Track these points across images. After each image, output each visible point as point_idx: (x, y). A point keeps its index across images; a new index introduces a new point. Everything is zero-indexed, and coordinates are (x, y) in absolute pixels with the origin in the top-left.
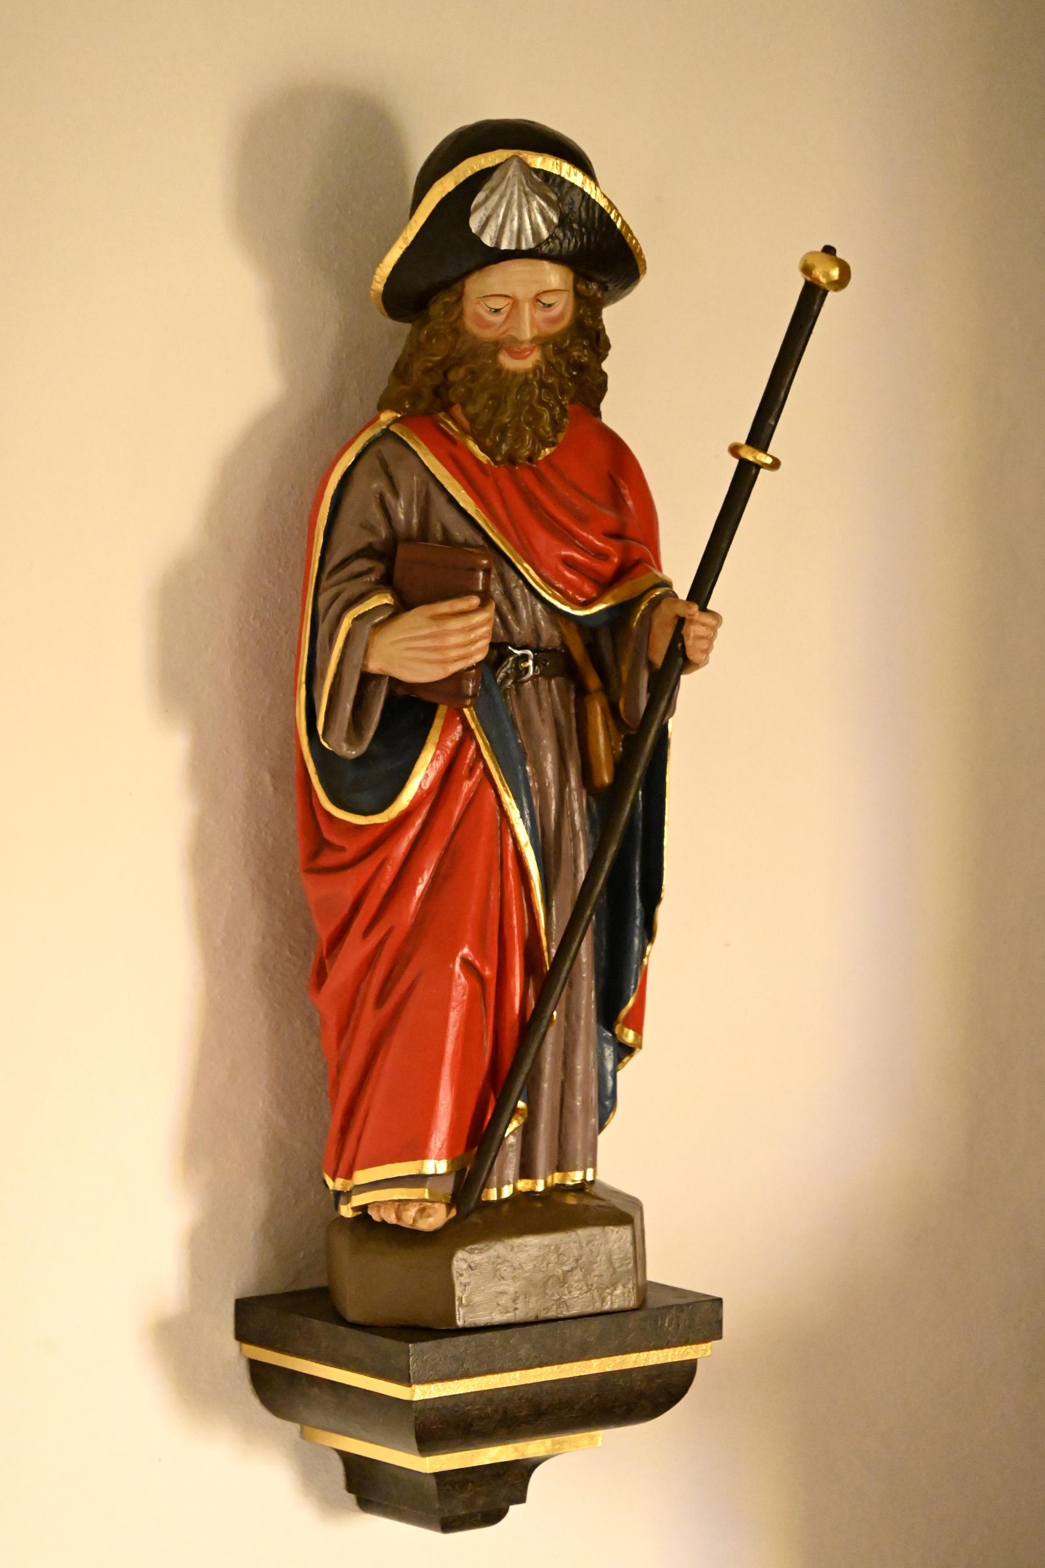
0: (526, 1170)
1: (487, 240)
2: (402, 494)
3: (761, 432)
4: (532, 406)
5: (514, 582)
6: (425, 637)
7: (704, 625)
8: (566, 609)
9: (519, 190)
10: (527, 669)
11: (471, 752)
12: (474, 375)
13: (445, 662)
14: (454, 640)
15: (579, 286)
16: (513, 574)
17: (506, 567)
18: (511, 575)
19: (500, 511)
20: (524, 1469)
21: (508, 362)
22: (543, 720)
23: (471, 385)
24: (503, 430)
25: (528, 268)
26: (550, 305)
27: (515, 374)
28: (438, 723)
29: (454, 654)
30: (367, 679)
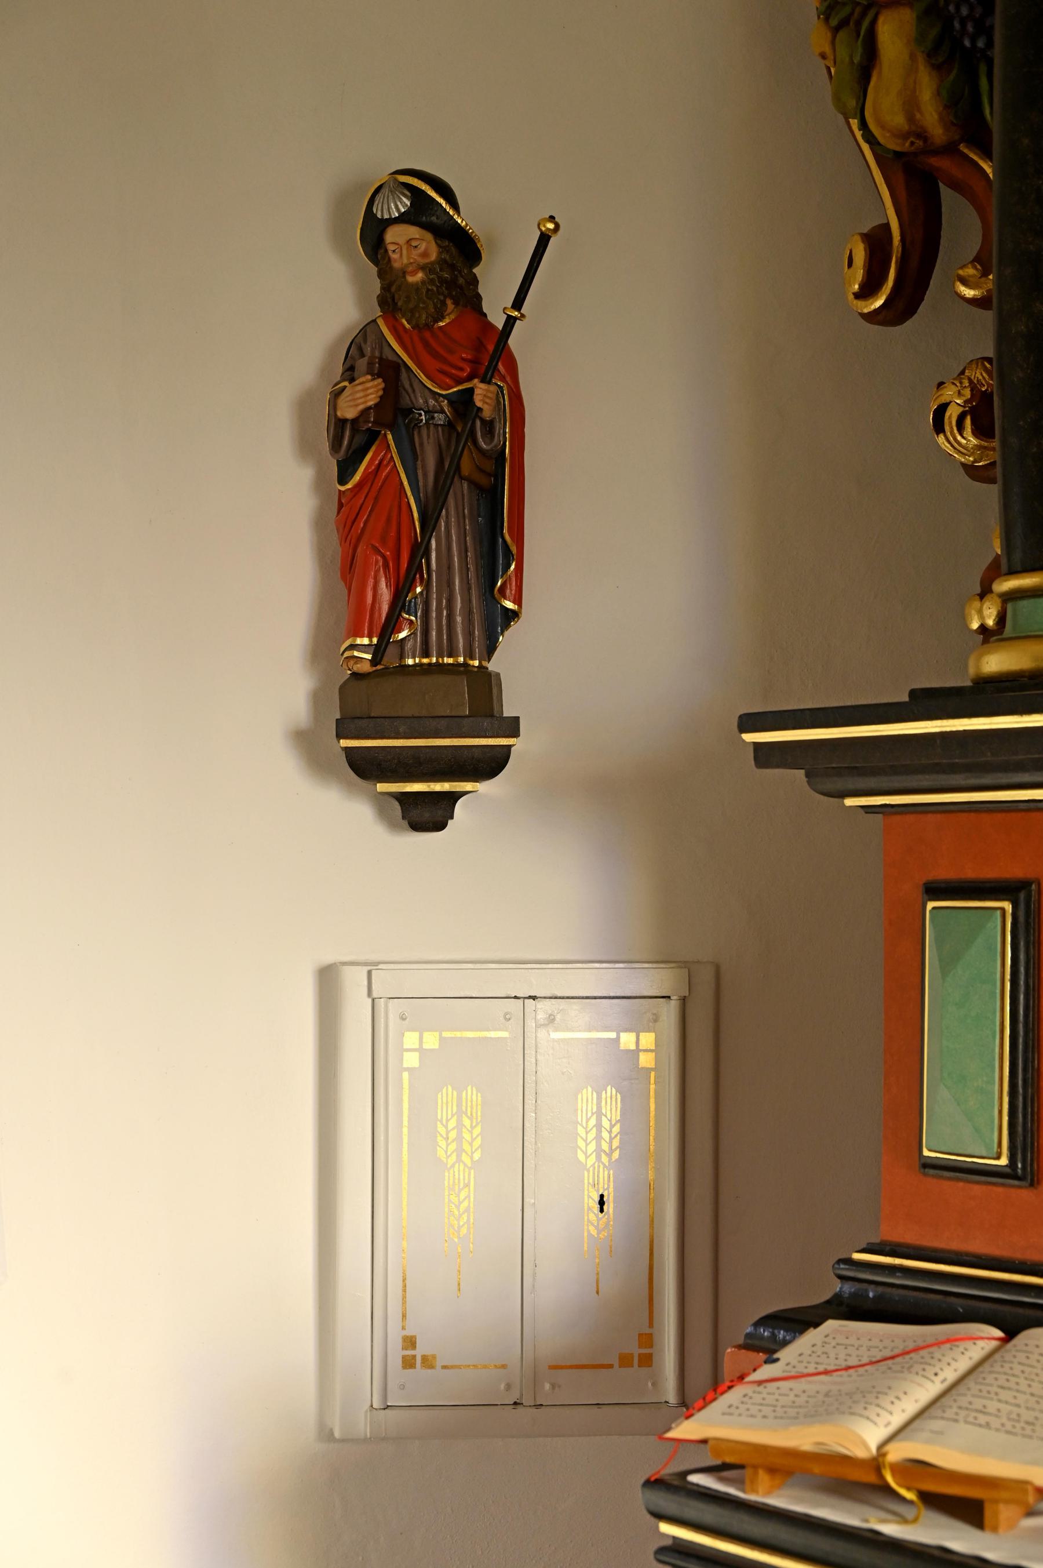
0: (426, 654)
2: (369, 343)
5: (412, 376)
13: (357, 405)
14: (359, 395)
20: (453, 798)
21: (410, 279)
28: (377, 443)
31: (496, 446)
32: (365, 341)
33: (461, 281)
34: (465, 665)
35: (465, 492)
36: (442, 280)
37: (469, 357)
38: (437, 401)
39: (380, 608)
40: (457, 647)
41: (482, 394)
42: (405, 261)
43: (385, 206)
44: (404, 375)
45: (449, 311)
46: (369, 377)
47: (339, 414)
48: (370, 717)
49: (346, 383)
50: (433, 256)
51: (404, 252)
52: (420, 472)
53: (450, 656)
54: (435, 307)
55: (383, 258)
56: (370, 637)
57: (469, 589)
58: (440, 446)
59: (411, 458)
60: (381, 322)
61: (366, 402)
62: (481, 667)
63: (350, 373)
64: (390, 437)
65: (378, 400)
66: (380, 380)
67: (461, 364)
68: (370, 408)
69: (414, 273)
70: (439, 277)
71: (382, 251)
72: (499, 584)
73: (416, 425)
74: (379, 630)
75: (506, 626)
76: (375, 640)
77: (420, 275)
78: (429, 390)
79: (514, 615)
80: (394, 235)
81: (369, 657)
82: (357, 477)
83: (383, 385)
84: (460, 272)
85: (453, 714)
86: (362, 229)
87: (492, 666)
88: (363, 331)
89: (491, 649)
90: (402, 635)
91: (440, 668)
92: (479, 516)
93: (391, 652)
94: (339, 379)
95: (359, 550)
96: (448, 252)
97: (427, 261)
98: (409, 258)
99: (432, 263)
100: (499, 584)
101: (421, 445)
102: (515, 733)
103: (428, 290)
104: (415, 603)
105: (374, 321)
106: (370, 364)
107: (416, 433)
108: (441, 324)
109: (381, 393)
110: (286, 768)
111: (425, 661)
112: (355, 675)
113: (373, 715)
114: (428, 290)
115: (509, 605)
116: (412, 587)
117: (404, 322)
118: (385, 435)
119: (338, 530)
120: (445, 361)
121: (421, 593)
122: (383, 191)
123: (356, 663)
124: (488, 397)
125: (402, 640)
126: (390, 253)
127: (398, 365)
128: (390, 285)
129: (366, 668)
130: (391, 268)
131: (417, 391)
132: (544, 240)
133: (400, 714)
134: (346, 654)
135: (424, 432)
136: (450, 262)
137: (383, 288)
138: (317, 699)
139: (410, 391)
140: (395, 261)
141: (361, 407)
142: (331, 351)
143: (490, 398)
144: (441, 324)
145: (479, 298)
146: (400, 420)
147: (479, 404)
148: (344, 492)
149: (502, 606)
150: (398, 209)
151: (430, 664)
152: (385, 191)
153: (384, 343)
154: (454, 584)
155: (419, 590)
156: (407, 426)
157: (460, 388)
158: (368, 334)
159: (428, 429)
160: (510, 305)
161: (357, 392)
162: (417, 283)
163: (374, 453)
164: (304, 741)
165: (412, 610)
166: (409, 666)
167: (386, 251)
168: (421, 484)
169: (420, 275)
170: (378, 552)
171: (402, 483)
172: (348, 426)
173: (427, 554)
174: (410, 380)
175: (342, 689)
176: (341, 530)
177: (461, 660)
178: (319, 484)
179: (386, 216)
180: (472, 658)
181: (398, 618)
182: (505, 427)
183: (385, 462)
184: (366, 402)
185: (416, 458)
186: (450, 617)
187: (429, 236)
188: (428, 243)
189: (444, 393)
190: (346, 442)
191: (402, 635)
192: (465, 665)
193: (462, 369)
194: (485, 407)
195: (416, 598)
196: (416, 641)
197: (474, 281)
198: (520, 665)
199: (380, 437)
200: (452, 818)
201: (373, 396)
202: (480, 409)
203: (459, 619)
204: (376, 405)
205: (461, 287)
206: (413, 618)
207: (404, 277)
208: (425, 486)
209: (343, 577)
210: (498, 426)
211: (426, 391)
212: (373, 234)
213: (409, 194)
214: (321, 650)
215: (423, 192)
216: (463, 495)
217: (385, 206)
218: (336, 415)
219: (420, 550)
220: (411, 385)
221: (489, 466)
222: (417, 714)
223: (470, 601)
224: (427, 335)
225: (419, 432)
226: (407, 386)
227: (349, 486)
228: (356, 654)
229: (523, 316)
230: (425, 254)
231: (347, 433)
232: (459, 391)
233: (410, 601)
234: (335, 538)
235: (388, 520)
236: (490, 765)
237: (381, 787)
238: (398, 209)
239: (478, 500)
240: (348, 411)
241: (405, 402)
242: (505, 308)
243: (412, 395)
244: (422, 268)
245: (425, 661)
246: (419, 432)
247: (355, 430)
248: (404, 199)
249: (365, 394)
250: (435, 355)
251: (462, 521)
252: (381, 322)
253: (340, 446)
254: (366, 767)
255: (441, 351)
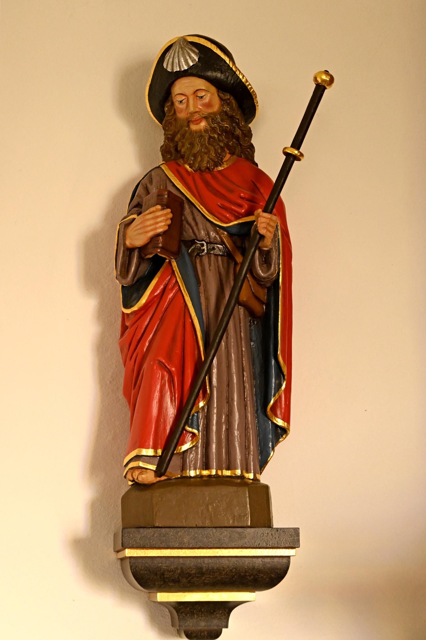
0: (207, 466)
1: (169, 70)
2: (154, 184)
3: (297, 142)
4: (206, 145)
5: (195, 211)
7: (264, 217)
8: (218, 223)
10: (204, 250)
11: (174, 281)
12: (183, 136)
14: (148, 223)
15: (220, 94)
16: (196, 210)
17: (194, 208)
18: (195, 211)
19: (195, 191)
20: (227, 608)
21: (194, 127)
24: (195, 156)
28: (162, 270)
29: (149, 228)
31: (272, 274)
32: (151, 182)
33: (238, 132)
34: (242, 477)
35: (242, 317)
36: (224, 130)
37: (246, 196)
38: (217, 233)
39: (165, 422)
40: (235, 460)
41: (264, 221)
42: (192, 109)
43: (176, 60)
44: (187, 210)
45: (225, 159)
46: (159, 207)
47: (128, 243)
48: (155, 527)
53: (228, 469)
56: (155, 448)
57: (246, 406)
59: (195, 283)
61: (156, 229)
62: (255, 479)
63: (137, 206)
64: (174, 264)
65: (166, 228)
66: (169, 210)
67: (240, 201)
68: (158, 235)
70: (220, 127)
71: (169, 104)
72: (272, 402)
73: (198, 254)
74: (164, 442)
75: (276, 441)
76: (160, 452)
77: (203, 124)
78: (210, 226)
79: (284, 431)
80: (183, 87)
81: (154, 467)
83: (171, 216)
85: (236, 524)
86: (151, 85)
87: (264, 479)
88: (149, 176)
89: (263, 463)
90: (185, 447)
91: (218, 480)
92: (251, 340)
93: (176, 461)
95: (145, 366)
96: (228, 104)
97: (210, 111)
98: (195, 106)
99: (214, 114)
100: (272, 402)
101: (203, 271)
102: (294, 544)
103: (210, 137)
104: (198, 417)
105: (159, 167)
106: (160, 195)
107: (198, 261)
108: (220, 168)
109: (169, 222)
110: (65, 574)
111: (205, 473)
112: (137, 486)
113: (157, 524)
114: (210, 137)
115: (280, 422)
116: (195, 403)
118: (170, 263)
119: (122, 351)
121: (203, 408)
122: (173, 48)
123: (141, 473)
125: (185, 452)
126: (177, 104)
128: (174, 135)
129: (149, 478)
131: (201, 226)
132: (319, 90)
133: (184, 525)
134: (131, 465)
135: (206, 260)
136: (230, 113)
138: (96, 508)
139: (193, 223)
140: (181, 111)
141: (151, 234)
142: (116, 199)
143: (272, 227)
144: (220, 168)
145: (252, 147)
146: (184, 249)
147: (262, 231)
149: (273, 423)
151: (210, 476)
152: (176, 48)
153: (168, 182)
154: (233, 400)
155: (201, 404)
156: (190, 255)
157: (240, 221)
158: (153, 177)
160: (290, 146)
161: (148, 220)
162: (201, 131)
163: (162, 276)
164: (83, 549)
165: (195, 423)
166: (191, 477)
167: (173, 104)
169: (203, 124)
170: (163, 367)
171: (186, 305)
172: (136, 254)
173: (209, 372)
174: (193, 214)
175: (125, 499)
176: (126, 350)
177: (238, 472)
178: (102, 313)
180: (248, 471)
181: (182, 432)
182: (279, 259)
183: (170, 286)
186: (229, 430)
187: (213, 89)
188: (212, 94)
189: (225, 225)
191: (185, 447)
192: (242, 477)
193: (240, 206)
194: (269, 236)
195: (198, 412)
196: (197, 453)
197: (249, 134)
198: (290, 478)
199: (165, 265)
200: (227, 627)
201: (163, 224)
202: (262, 237)
203: (236, 433)
204: (165, 232)
205: (238, 138)
206: (196, 431)
207: (188, 126)
208: (207, 308)
209: (127, 393)
211: (209, 225)
212: (162, 87)
214: (100, 463)
215: (210, 49)
216: (240, 319)
217: (176, 60)
218: (125, 244)
219: (201, 368)
220: (194, 219)
221: (263, 294)
222: (201, 525)
223: (246, 417)
224: (208, 177)
225: (201, 261)
226: (190, 219)
227: (135, 308)
228: (141, 464)
230: (209, 105)
231: (135, 261)
232: (239, 224)
233: (193, 415)
234: (117, 357)
235: (173, 339)
236: (267, 576)
237: (163, 597)
239: (250, 326)
240: (137, 238)
241: (188, 234)
242: (285, 148)
243: (195, 228)
244: (206, 118)
245: (205, 473)
246: (201, 261)
247: (141, 259)
248: (193, 55)
249: (157, 221)
250: (217, 193)
251: (239, 341)
253: (128, 271)
254: (148, 577)
255: (223, 191)
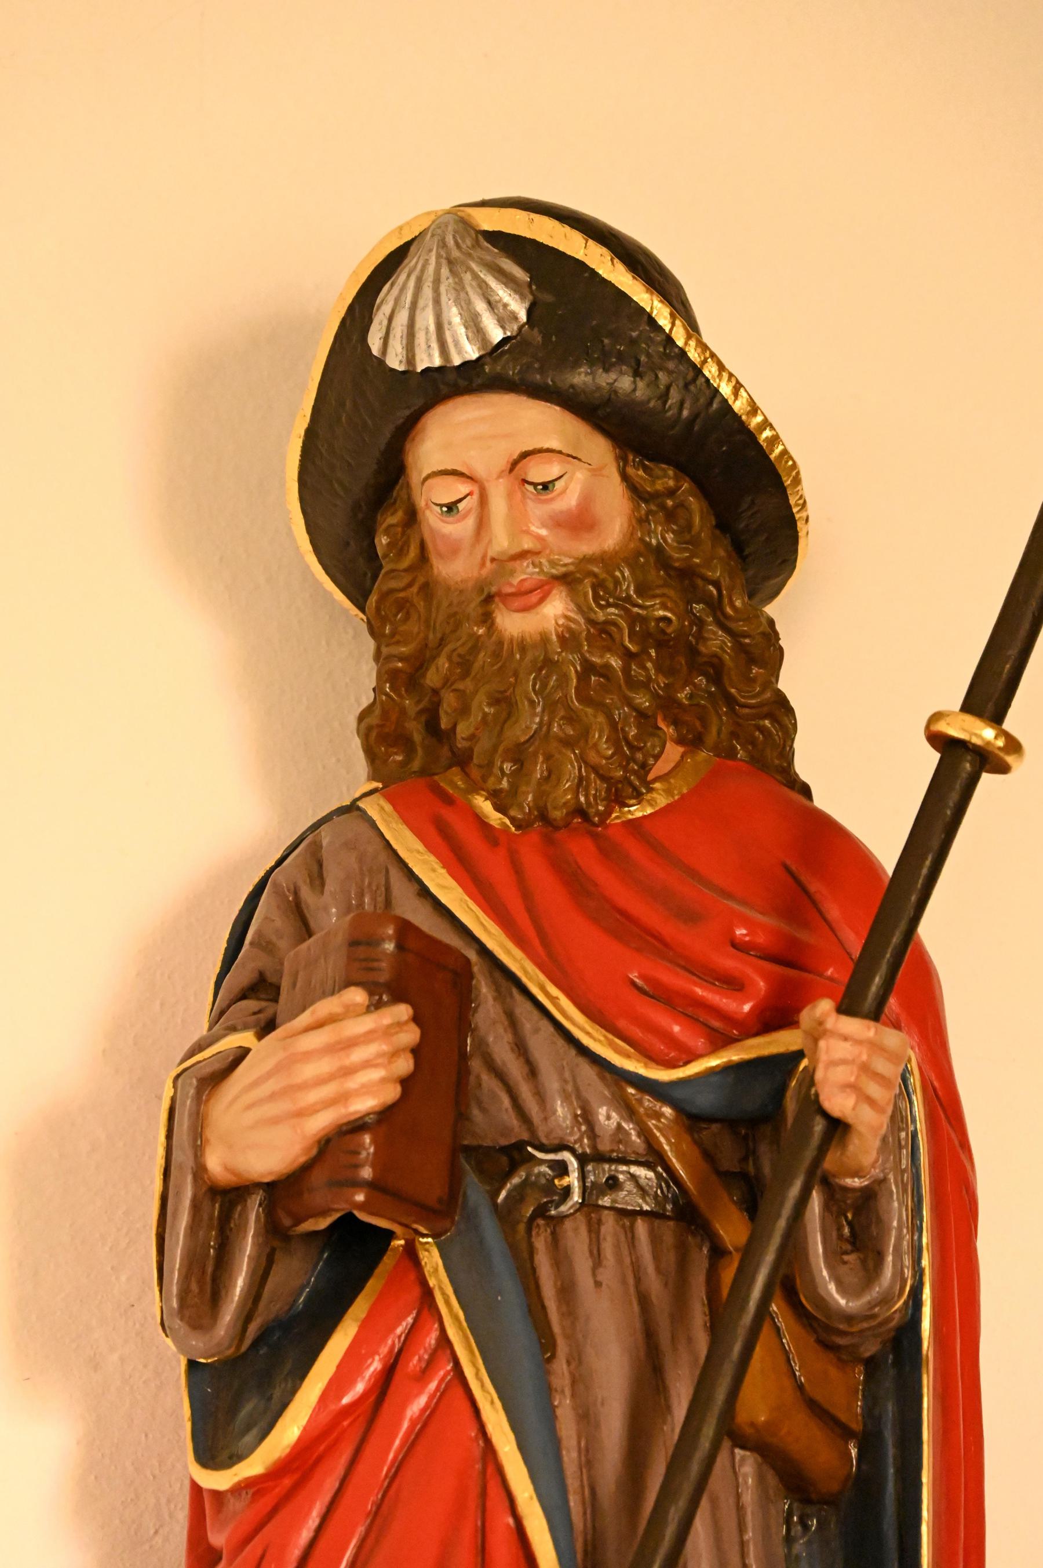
1: (395, 361)
2: (330, 886)
4: (569, 708)
6: (269, 1075)
7: (846, 1038)
9: (439, 256)
10: (567, 1191)
11: (432, 1339)
12: (464, 665)
13: (302, 1114)
14: (310, 1070)
15: (630, 471)
21: (512, 624)
22: (598, 1284)
23: (460, 686)
25: (486, 412)
26: (546, 486)
27: (523, 646)
28: (373, 1286)
29: (313, 1096)
30: (224, 1199)
31: (886, 1300)
32: (318, 879)
35: (748, 1498)
36: (653, 636)
38: (630, 1111)
41: (846, 1059)
42: (501, 541)
43: (426, 319)
46: (357, 996)
49: (245, 1038)
50: (614, 530)
51: (498, 506)
52: (565, 1407)
54: (617, 736)
55: (399, 548)
58: (644, 1301)
59: (531, 1345)
60: (376, 809)
61: (343, 1098)
63: (255, 991)
64: (431, 1259)
65: (392, 1093)
66: (403, 1011)
67: (730, 963)
68: (356, 1127)
69: (529, 597)
70: (633, 620)
71: (394, 518)
78: (595, 1078)
80: (462, 443)
82: (289, 1430)
83: (411, 1035)
84: (715, 606)
88: (307, 851)
94: (202, 1029)
96: (670, 516)
97: (587, 547)
99: (605, 560)
101: (567, 1291)
103: (588, 668)
105: (352, 808)
106: (360, 942)
107: (541, 1243)
108: (637, 811)
109: (405, 1065)
114: (588, 668)
117: (485, 806)
118: (411, 1252)
120: (658, 945)
122: (411, 261)
124: (877, 1077)
126: (432, 519)
127: (462, 975)
128: (420, 662)
130: (427, 589)
135: (576, 1239)
137: (388, 675)
139: (515, 1069)
140: (454, 549)
141: (321, 1122)
144: (637, 811)
146: (474, 1189)
148: (217, 1495)
150: (476, 330)
152: (426, 262)
156: (505, 1215)
159: (594, 1229)
161: (308, 1056)
163: (365, 1325)
167: (412, 516)
168: (570, 1457)
169: (556, 609)
171: (489, 1450)
174: (513, 1023)
179: (428, 359)
183: (413, 1364)
184: (343, 1098)
185: (546, 1344)
187: (598, 449)
188: (596, 472)
190: (240, 1283)
193: (734, 984)
197: (765, 651)
199: (388, 1262)
201: (375, 1074)
202: (838, 1128)
204: (386, 1114)
205: (715, 671)
207: (487, 618)
208: (588, 1461)
210: (895, 1210)
211: (587, 1072)
213: (520, 274)
216: (740, 1508)
217: (426, 319)
218: (200, 1170)
220: (521, 1048)
221: (845, 1392)
224: (581, 851)
227: (253, 1466)
229: (1014, 746)
230: (579, 522)
231: (248, 1247)
238: (476, 330)
240: (260, 1138)
241: (494, 1119)
242: (936, 717)
243: (525, 1091)
244: (567, 580)
247: (276, 1235)
248: (503, 294)
249: (345, 1061)
250: (625, 927)
252: (376, 809)
253: (216, 1296)
